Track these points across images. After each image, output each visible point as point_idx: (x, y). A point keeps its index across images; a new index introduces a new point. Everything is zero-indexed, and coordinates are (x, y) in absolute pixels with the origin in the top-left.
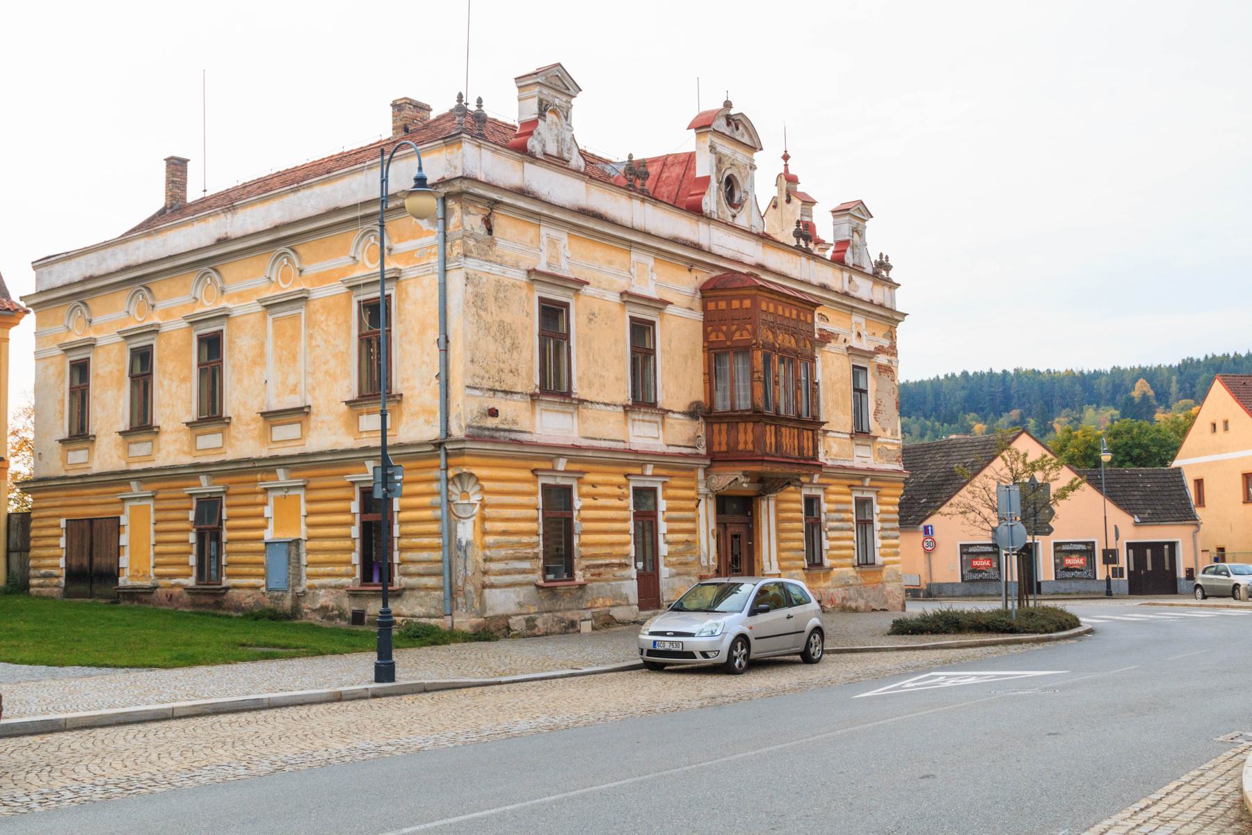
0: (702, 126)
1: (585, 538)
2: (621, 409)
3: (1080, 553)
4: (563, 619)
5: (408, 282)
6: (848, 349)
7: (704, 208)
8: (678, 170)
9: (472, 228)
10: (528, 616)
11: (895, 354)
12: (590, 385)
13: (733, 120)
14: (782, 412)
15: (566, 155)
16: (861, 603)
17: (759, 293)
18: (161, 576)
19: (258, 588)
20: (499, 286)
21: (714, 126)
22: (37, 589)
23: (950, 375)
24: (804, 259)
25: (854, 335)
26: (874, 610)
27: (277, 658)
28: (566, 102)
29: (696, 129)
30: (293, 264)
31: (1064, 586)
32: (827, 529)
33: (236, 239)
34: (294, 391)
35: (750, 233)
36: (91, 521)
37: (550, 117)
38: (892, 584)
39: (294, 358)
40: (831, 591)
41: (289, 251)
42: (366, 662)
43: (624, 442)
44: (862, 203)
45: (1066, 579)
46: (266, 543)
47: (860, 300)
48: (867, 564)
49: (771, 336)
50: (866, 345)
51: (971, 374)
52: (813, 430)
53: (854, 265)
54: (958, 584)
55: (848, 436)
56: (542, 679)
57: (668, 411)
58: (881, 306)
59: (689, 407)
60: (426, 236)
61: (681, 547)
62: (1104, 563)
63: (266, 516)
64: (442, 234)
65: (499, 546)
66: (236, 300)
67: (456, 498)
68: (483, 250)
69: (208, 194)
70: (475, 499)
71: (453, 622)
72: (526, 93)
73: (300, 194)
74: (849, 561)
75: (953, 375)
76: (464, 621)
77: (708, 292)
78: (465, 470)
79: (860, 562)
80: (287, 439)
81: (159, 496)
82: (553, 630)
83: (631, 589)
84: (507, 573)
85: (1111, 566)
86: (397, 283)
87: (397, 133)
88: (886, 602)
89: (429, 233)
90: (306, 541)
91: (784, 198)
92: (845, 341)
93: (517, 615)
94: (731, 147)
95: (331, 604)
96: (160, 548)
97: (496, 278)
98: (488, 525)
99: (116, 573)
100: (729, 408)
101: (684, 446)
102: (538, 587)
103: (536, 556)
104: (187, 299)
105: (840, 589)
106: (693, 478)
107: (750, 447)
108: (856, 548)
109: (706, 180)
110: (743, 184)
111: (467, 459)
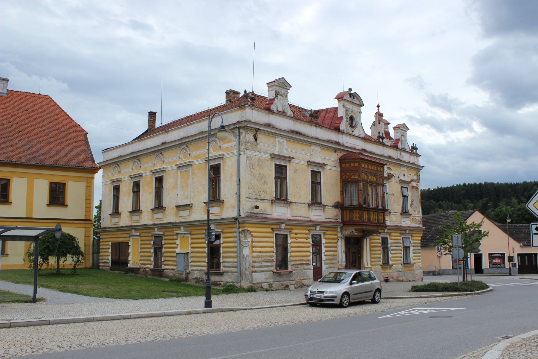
0: (340, 98)
1: (292, 254)
2: (307, 205)
3: (499, 257)
4: (283, 284)
5: (226, 159)
6: (399, 180)
7: (341, 128)
8: (332, 114)
9: (249, 139)
10: (270, 283)
11: (419, 182)
12: (295, 196)
13: (352, 95)
14: (371, 206)
15: (286, 111)
16: (404, 278)
17: (361, 161)
18: (142, 264)
19: (174, 270)
20: (259, 160)
21: (345, 98)
22: (102, 267)
23: (458, 185)
24: (381, 147)
25: (402, 175)
26: (410, 281)
27: (174, 297)
28: (286, 91)
29: (338, 99)
30: (187, 152)
31: (492, 270)
32: (391, 250)
33: (168, 143)
34: (187, 198)
35: (359, 137)
36: (119, 243)
37: (279, 97)
38: (417, 271)
39: (187, 186)
40: (392, 274)
41: (186, 147)
42: (202, 299)
43: (308, 217)
44: (405, 124)
45: (494, 268)
46: (177, 254)
47: (404, 162)
48: (407, 263)
49: (366, 177)
50: (407, 179)
51: (467, 184)
52: (383, 213)
53: (402, 148)
54: (451, 270)
55: (400, 214)
56: (268, 308)
57: (326, 206)
58: (413, 164)
59: (335, 204)
60: (233, 142)
61: (331, 257)
62: (508, 262)
63: (177, 244)
64: (238, 142)
65: (259, 257)
66: (168, 165)
67: (242, 239)
68: (253, 147)
69: (162, 125)
70: (249, 239)
71: (241, 285)
72: (271, 89)
73: (190, 127)
74: (400, 262)
75: (460, 185)
76: (245, 284)
77: (342, 161)
78: (245, 229)
79: (405, 262)
80: (185, 216)
81: (142, 235)
82: (279, 288)
83: (311, 273)
84: (262, 267)
85: (511, 263)
86: (223, 159)
87: (227, 102)
88: (415, 278)
89: (234, 141)
90: (190, 253)
91: (378, 122)
92: (398, 177)
93: (265, 282)
94: (351, 105)
95: (199, 277)
96: (142, 254)
97: (258, 157)
98: (254, 249)
99: (127, 262)
100: (350, 204)
101: (332, 219)
102: (274, 272)
103: (273, 261)
104: (152, 164)
105: (396, 273)
106: (336, 231)
107: (358, 219)
108: (403, 257)
109: (342, 118)
110: (356, 119)
111: (246, 225)
